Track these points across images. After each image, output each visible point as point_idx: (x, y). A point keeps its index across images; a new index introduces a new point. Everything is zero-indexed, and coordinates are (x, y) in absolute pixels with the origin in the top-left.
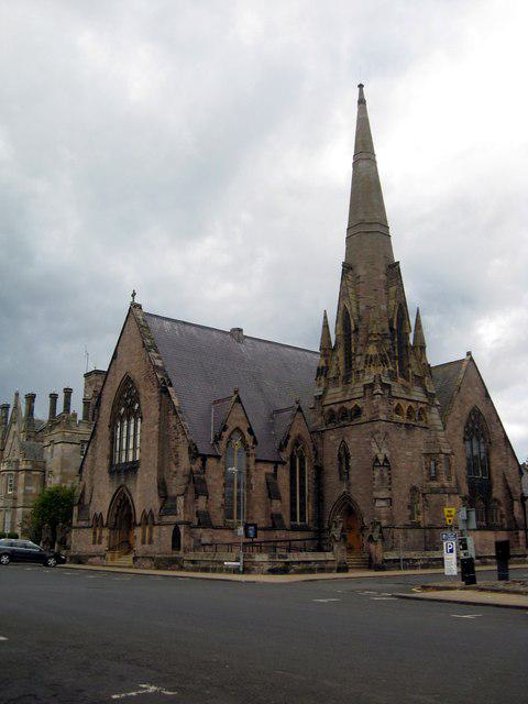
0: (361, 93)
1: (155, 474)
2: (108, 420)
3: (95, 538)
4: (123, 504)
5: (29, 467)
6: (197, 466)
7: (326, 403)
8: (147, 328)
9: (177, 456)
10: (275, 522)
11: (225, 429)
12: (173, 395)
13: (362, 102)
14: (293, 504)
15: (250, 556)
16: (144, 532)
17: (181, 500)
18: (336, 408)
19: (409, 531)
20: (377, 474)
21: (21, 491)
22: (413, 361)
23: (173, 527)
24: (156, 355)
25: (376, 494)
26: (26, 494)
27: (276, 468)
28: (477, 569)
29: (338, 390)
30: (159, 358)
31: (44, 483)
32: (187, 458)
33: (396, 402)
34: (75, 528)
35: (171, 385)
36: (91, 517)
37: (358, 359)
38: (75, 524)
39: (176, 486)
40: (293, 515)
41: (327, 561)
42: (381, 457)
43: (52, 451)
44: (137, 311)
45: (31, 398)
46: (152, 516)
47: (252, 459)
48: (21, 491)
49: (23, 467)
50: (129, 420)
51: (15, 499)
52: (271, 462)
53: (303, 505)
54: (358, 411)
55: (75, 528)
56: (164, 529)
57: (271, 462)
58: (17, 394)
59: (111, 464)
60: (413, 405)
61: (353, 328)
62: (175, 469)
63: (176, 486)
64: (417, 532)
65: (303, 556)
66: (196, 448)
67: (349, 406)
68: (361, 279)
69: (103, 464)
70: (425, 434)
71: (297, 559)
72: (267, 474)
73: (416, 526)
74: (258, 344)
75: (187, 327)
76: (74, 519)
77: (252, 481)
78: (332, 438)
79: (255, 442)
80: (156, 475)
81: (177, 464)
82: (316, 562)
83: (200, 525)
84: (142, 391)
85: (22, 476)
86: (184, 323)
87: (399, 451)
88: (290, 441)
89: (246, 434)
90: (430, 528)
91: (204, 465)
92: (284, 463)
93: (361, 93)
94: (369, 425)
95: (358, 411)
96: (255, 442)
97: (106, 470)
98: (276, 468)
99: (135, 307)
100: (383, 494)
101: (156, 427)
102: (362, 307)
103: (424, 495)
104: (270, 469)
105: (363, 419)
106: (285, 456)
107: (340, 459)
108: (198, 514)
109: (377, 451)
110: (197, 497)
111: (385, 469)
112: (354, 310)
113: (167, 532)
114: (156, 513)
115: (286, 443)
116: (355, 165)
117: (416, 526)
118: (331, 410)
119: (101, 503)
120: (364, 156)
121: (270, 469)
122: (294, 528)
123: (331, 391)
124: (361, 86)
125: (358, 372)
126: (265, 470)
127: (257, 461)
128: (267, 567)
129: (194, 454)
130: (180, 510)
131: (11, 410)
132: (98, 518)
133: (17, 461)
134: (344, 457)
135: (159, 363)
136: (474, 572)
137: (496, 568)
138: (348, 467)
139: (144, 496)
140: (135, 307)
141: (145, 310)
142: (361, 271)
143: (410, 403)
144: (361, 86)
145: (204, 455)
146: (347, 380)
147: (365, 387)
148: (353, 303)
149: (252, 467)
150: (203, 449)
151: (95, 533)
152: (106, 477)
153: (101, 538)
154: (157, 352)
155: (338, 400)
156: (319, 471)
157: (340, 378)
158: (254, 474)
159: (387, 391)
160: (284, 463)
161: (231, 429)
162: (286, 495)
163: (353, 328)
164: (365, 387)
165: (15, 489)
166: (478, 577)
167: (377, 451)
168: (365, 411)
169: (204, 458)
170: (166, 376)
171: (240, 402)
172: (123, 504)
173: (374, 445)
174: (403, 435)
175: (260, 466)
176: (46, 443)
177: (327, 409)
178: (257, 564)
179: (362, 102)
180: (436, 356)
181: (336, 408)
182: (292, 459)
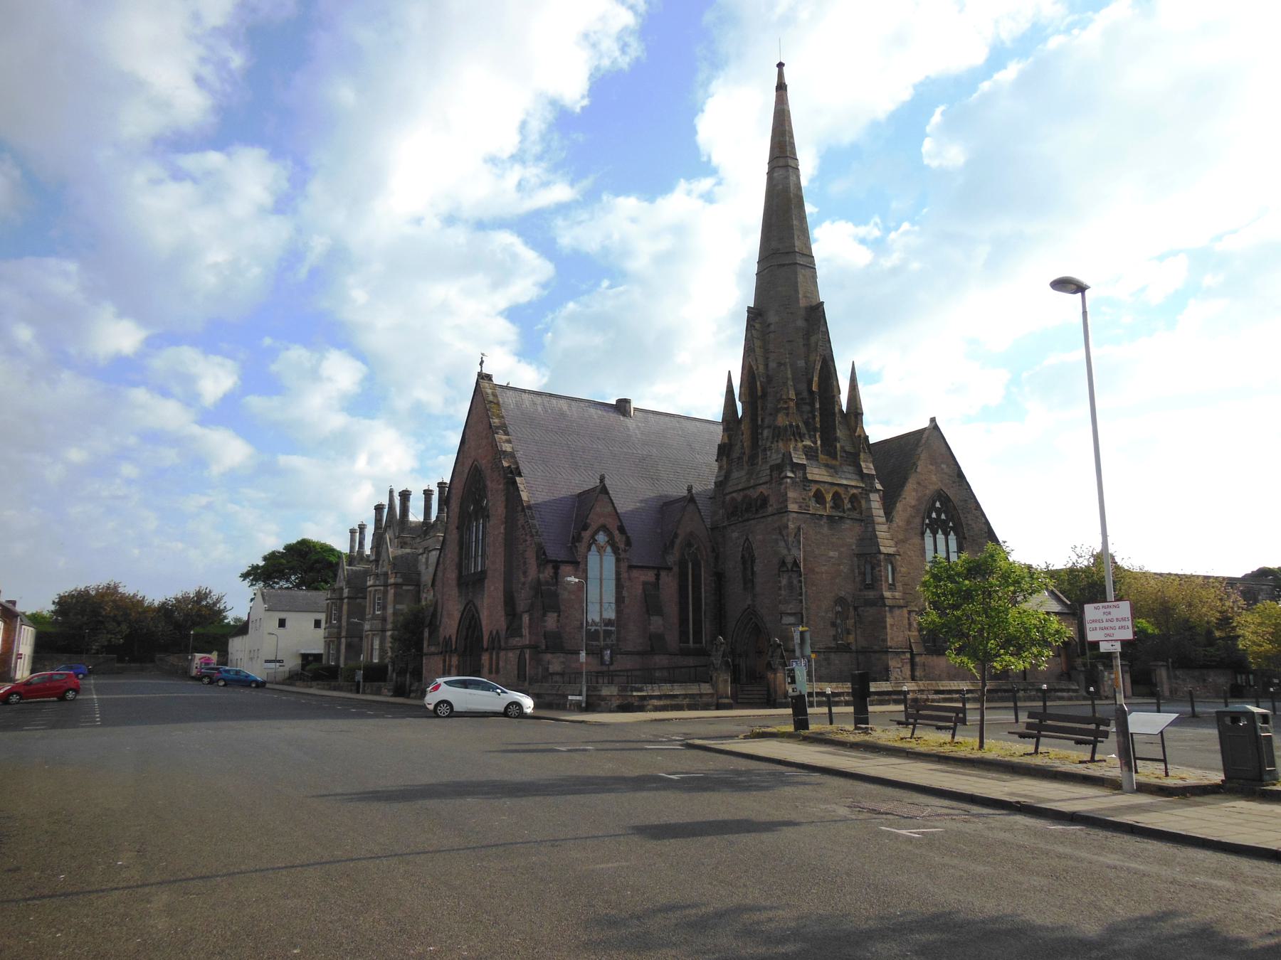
0: (781, 75)
1: (501, 586)
2: (456, 521)
3: (444, 666)
4: (470, 622)
5: (400, 580)
6: (548, 572)
7: (729, 490)
8: (498, 404)
9: (525, 563)
10: (655, 644)
11: (585, 528)
12: (521, 487)
13: (781, 87)
14: (683, 621)
15: (595, 689)
16: (491, 659)
17: (526, 618)
18: (739, 497)
19: (833, 656)
20: (784, 582)
21: (390, 611)
22: (840, 433)
23: (518, 652)
24: (504, 437)
25: (782, 607)
26: (395, 614)
27: (658, 576)
28: (810, 710)
29: (743, 473)
30: (509, 441)
31: (419, 600)
32: (534, 568)
33: (814, 488)
34: (426, 655)
35: (520, 475)
36: (441, 640)
37: (766, 433)
38: (425, 650)
39: (523, 598)
40: (683, 635)
41: (701, 695)
42: (789, 560)
43: (427, 559)
44: (485, 384)
45: (405, 495)
46: (499, 637)
47: (624, 565)
48: (390, 611)
49: (392, 581)
50: (477, 520)
51: (384, 619)
52: (653, 568)
53: (697, 623)
54: (764, 501)
55: (426, 655)
56: (510, 654)
57: (653, 568)
58: (391, 492)
59: (460, 577)
60: (841, 491)
61: (759, 393)
62: (523, 579)
63: (523, 598)
64: (846, 656)
65: (666, 689)
66: (544, 553)
67: (754, 494)
68: (772, 328)
69: (452, 575)
70: (858, 529)
71: (656, 693)
72: (645, 583)
73: (845, 648)
74: (651, 417)
75: (554, 401)
76: (425, 645)
77: (625, 593)
78: (735, 535)
79: (628, 543)
80: (501, 588)
81: (525, 573)
82: (686, 696)
83: (547, 650)
84: (488, 483)
85: (391, 592)
86: (551, 395)
87: (817, 552)
88: (678, 541)
89: (616, 533)
90: (864, 651)
91: (556, 574)
92: (670, 569)
93: (781, 75)
94: (776, 517)
95: (764, 501)
96: (628, 543)
97: (454, 583)
98: (658, 576)
99: (483, 377)
100: (791, 608)
101: (503, 527)
102: (772, 365)
103: (856, 608)
104: (649, 576)
105: (770, 510)
106: (672, 559)
107: (744, 563)
108: (545, 636)
109: (785, 552)
110: (544, 615)
111: (794, 575)
112: (761, 368)
113: (512, 656)
114: (503, 634)
115: (672, 543)
116: (770, 174)
117: (845, 648)
118: (733, 499)
119: (450, 625)
120: (782, 162)
121: (649, 576)
122: (684, 653)
123: (735, 475)
124: (780, 65)
125: (765, 450)
126: (643, 578)
127: (631, 567)
128: (616, 703)
129: (543, 560)
130: (525, 631)
131: (386, 511)
132: (447, 641)
133: (386, 574)
134: (748, 559)
135: (507, 447)
136: (806, 714)
137: (851, 709)
138: (753, 573)
139: (491, 616)
140: (483, 377)
141: (496, 381)
142: (772, 318)
143: (836, 488)
144: (780, 65)
145: (556, 561)
146: (753, 459)
147: (772, 468)
148: (761, 360)
149: (624, 575)
150: (554, 552)
151: (444, 661)
152: (454, 592)
153: (450, 666)
154: (506, 433)
155: (740, 487)
156: (719, 577)
157: (745, 458)
158: (627, 584)
159: (800, 474)
160: (670, 569)
161: (594, 527)
162: (672, 609)
163: (759, 393)
164: (772, 468)
165: (384, 608)
166: (1114, 714)
167: (785, 552)
168: (772, 500)
169: (556, 565)
170: (516, 463)
171: (607, 493)
172: (470, 622)
173: (782, 544)
174: (825, 530)
175: (635, 573)
176: (421, 551)
177: (728, 498)
178: (603, 698)
179: (781, 87)
180: (877, 429)
181: (739, 497)
182: (682, 564)
